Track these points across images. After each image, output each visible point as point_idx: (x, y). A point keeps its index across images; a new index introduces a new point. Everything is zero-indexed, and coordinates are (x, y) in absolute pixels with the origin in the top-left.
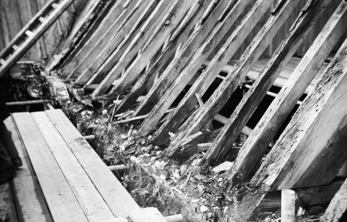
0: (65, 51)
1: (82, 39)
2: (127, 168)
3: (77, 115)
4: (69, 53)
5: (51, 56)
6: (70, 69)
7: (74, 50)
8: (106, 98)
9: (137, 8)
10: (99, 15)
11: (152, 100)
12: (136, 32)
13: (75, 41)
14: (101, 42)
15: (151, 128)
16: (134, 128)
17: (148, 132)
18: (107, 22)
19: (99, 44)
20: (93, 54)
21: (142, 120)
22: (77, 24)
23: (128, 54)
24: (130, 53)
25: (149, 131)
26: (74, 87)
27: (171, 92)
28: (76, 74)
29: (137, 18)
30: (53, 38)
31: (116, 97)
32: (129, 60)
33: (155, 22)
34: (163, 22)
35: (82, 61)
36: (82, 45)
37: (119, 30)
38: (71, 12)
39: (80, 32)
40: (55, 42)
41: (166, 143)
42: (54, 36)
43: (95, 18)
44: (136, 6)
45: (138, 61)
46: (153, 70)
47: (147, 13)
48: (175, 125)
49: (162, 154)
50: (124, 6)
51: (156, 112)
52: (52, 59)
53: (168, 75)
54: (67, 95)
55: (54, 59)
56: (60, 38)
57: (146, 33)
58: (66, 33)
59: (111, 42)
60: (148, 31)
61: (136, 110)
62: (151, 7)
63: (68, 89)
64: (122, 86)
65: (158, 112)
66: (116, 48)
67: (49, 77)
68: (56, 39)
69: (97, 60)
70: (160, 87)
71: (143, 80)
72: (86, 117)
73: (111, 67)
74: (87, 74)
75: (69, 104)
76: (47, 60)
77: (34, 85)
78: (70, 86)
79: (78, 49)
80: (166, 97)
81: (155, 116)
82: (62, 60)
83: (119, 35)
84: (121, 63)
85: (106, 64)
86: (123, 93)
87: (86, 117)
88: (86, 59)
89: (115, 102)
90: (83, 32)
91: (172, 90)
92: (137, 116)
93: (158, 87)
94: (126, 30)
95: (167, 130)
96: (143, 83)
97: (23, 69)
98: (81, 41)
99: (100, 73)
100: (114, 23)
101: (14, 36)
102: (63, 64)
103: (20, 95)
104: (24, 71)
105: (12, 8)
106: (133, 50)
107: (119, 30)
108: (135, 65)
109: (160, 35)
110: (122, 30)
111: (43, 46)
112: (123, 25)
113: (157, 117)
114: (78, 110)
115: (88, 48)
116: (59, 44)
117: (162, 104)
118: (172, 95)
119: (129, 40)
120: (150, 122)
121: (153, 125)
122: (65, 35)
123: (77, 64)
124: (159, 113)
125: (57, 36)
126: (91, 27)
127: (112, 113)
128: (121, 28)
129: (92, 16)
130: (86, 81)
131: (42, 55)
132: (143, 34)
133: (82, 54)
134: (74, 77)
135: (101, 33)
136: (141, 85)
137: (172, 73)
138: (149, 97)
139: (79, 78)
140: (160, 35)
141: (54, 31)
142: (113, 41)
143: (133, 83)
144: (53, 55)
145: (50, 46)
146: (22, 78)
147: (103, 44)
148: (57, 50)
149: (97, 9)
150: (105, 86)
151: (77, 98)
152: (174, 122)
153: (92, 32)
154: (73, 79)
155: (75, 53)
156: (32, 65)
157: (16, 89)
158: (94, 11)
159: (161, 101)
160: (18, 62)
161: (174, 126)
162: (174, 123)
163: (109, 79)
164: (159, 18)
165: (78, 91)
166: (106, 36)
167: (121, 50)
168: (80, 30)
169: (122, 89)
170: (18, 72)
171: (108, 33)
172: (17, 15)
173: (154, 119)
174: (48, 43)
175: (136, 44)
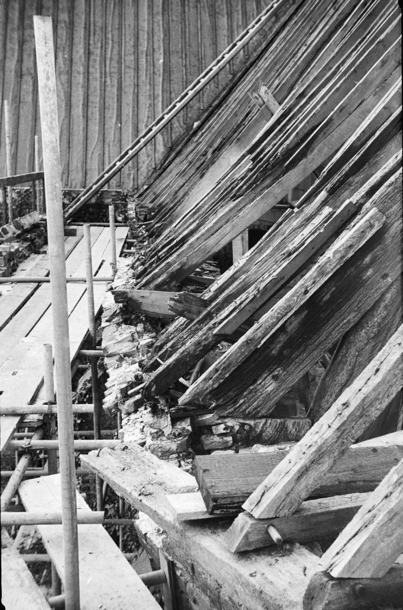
30: (146, 170)
40: (148, 174)
42: (147, 168)
58: (159, 167)
61: (282, 589)
63: (135, 210)
68: (149, 171)
75: (135, 222)
97: (114, 196)
105: (116, 143)
111: (136, 177)
125: (150, 168)
131: (134, 185)
145: (142, 178)
156: (120, 192)
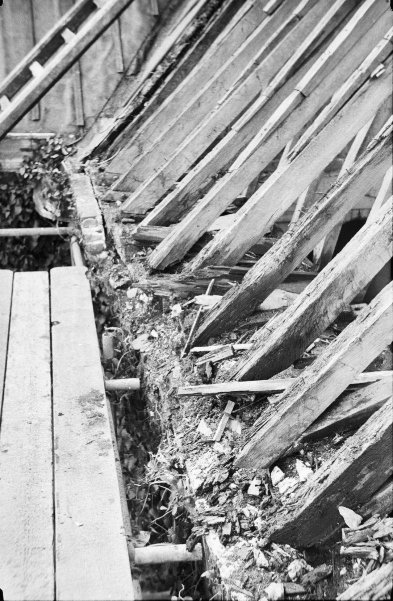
0: (124, 112)
1: (163, 86)
2: (196, 559)
3: (117, 294)
4: (130, 118)
5: (93, 120)
6: (121, 163)
7: (142, 113)
8: (176, 286)
9: (299, 17)
10: (207, 29)
11: (299, 332)
12: (285, 88)
13: (146, 90)
14: (198, 103)
15: (283, 446)
16: (233, 416)
17: (271, 458)
18: (221, 49)
19: (193, 108)
20: (175, 132)
21: (262, 398)
22: (159, 45)
23: (256, 153)
24: (263, 149)
25: (276, 456)
26: (118, 221)
27: (364, 335)
28: (129, 182)
29: (295, 44)
30: (102, 78)
31: (204, 283)
32: (256, 169)
33: (342, 63)
34: (364, 71)
35: (148, 148)
36: (160, 101)
37: (244, 77)
38: (150, 15)
39: (160, 68)
41: (324, 544)
42: (106, 72)
43: (199, 29)
44: (297, 11)
45: (278, 182)
46: (316, 223)
47: (323, 32)
48: (363, 481)
49: (305, 578)
50: (267, 8)
51: (304, 397)
52: (95, 129)
53: (360, 256)
54: (100, 239)
55: (99, 128)
56: (119, 77)
57: (313, 95)
58: (133, 67)
59: (219, 112)
60: (317, 91)
62: (336, 16)
64: (227, 249)
65: (312, 398)
66: (228, 130)
67: (78, 176)
69: (180, 154)
70: (329, 295)
71: (283, 252)
72: (134, 309)
73: (209, 180)
74: (153, 188)
76: (82, 130)
77: (45, 190)
78: (111, 213)
79: (151, 110)
80: (342, 352)
81: (300, 408)
82: (113, 136)
83: (243, 92)
84: (235, 177)
85: (197, 172)
86: (226, 273)
87: (134, 309)
88: (157, 145)
89: (199, 299)
90: (166, 68)
91: (367, 331)
92: (246, 378)
93: (323, 294)
94: (261, 77)
95: (332, 498)
96: (282, 259)
97: (27, 150)
98: (159, 91)
99: (178, 195)
100: (236, 54)
101: (15, 65)
102: (113, 145)
103: (18, 210)
104: (30, 154)
106: (270, 142)
107: (244, 77)
108: (270, 192)
109: (350, 108)
110: (251, 79)
111: (78, 95)
112: (257, 63)
113: (307, 413)
114: (120, 284)
115: (169, 113)
116: (114, 94)
117: (329, 373)
118: (365, 343)
119: (265, 109)
120: (282, 428)
121: (292, 435)
122: (130, 72)
123: (141, 151)
124: (314, 402)
126: (186, 57)
127: (190, 326)
128: (250, 71)
129: (192, 29)
130: (149, 207)
131: (74, 118)
132: (303, 96)
133: (153, 127)
134: (126, 190)
135: (200, 82)
136: (276, 266)
137: (374, 252)
138: (291, 321)
139: (133, 197)
140: (350, 108)
141: (106, 59)
142: (224, 105)
143: (259, 250)
144: (98, 118)
146: (22, 171)
147: (204, 107)
148: (108, 107)
149: (205, 11)
150: (186, 237)
151: (119, 251)
152: (363, 472)
153: (186, 70)
154: (122, 194)
155: (141, 120)
157: (9, 195)
158: (197, 16)
159: (326, 361)
160: (9, 134)
161: (358, 487)
162: (363, 476)
163: (198, 218)
164: (357, 52)
165: (124, 233)
166: (212, 88)
167: (242, 134)
168: (161, 62)
169: (226, 257)
170: (15, 156)
171: (217, 81)
172: (28, 17)
173: (295, 417)
174: (90, 87)
175: (280, 125)
